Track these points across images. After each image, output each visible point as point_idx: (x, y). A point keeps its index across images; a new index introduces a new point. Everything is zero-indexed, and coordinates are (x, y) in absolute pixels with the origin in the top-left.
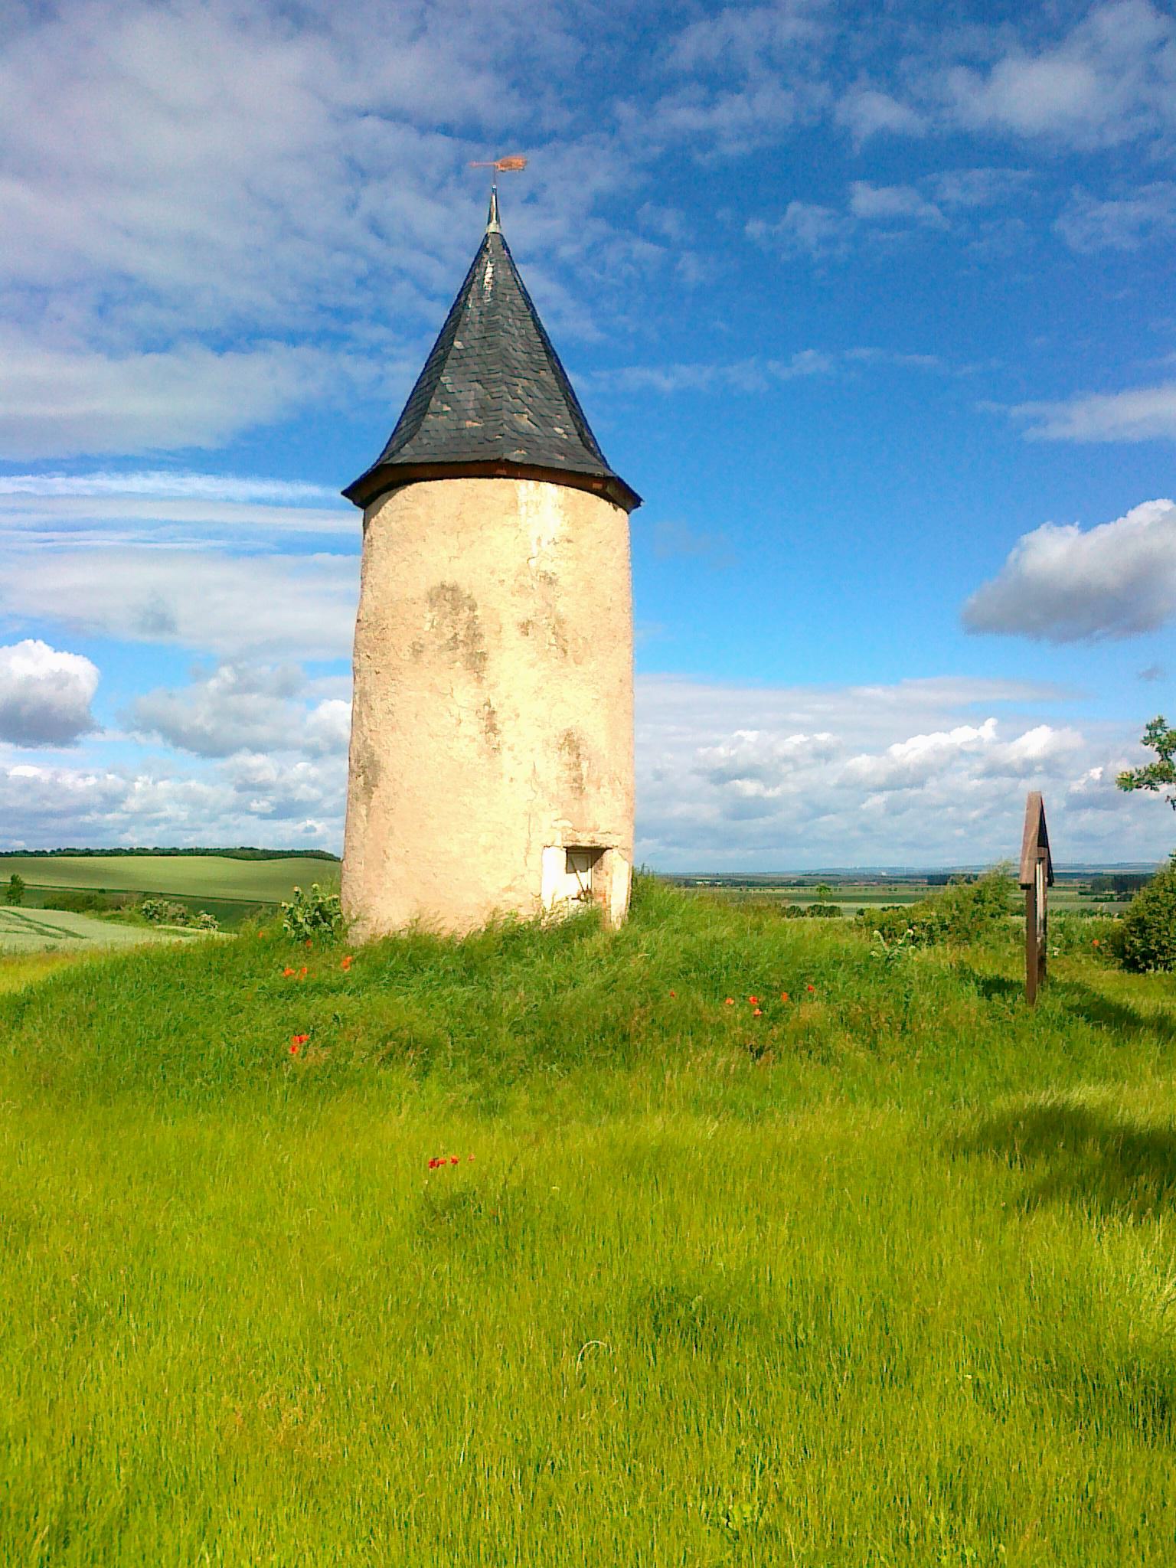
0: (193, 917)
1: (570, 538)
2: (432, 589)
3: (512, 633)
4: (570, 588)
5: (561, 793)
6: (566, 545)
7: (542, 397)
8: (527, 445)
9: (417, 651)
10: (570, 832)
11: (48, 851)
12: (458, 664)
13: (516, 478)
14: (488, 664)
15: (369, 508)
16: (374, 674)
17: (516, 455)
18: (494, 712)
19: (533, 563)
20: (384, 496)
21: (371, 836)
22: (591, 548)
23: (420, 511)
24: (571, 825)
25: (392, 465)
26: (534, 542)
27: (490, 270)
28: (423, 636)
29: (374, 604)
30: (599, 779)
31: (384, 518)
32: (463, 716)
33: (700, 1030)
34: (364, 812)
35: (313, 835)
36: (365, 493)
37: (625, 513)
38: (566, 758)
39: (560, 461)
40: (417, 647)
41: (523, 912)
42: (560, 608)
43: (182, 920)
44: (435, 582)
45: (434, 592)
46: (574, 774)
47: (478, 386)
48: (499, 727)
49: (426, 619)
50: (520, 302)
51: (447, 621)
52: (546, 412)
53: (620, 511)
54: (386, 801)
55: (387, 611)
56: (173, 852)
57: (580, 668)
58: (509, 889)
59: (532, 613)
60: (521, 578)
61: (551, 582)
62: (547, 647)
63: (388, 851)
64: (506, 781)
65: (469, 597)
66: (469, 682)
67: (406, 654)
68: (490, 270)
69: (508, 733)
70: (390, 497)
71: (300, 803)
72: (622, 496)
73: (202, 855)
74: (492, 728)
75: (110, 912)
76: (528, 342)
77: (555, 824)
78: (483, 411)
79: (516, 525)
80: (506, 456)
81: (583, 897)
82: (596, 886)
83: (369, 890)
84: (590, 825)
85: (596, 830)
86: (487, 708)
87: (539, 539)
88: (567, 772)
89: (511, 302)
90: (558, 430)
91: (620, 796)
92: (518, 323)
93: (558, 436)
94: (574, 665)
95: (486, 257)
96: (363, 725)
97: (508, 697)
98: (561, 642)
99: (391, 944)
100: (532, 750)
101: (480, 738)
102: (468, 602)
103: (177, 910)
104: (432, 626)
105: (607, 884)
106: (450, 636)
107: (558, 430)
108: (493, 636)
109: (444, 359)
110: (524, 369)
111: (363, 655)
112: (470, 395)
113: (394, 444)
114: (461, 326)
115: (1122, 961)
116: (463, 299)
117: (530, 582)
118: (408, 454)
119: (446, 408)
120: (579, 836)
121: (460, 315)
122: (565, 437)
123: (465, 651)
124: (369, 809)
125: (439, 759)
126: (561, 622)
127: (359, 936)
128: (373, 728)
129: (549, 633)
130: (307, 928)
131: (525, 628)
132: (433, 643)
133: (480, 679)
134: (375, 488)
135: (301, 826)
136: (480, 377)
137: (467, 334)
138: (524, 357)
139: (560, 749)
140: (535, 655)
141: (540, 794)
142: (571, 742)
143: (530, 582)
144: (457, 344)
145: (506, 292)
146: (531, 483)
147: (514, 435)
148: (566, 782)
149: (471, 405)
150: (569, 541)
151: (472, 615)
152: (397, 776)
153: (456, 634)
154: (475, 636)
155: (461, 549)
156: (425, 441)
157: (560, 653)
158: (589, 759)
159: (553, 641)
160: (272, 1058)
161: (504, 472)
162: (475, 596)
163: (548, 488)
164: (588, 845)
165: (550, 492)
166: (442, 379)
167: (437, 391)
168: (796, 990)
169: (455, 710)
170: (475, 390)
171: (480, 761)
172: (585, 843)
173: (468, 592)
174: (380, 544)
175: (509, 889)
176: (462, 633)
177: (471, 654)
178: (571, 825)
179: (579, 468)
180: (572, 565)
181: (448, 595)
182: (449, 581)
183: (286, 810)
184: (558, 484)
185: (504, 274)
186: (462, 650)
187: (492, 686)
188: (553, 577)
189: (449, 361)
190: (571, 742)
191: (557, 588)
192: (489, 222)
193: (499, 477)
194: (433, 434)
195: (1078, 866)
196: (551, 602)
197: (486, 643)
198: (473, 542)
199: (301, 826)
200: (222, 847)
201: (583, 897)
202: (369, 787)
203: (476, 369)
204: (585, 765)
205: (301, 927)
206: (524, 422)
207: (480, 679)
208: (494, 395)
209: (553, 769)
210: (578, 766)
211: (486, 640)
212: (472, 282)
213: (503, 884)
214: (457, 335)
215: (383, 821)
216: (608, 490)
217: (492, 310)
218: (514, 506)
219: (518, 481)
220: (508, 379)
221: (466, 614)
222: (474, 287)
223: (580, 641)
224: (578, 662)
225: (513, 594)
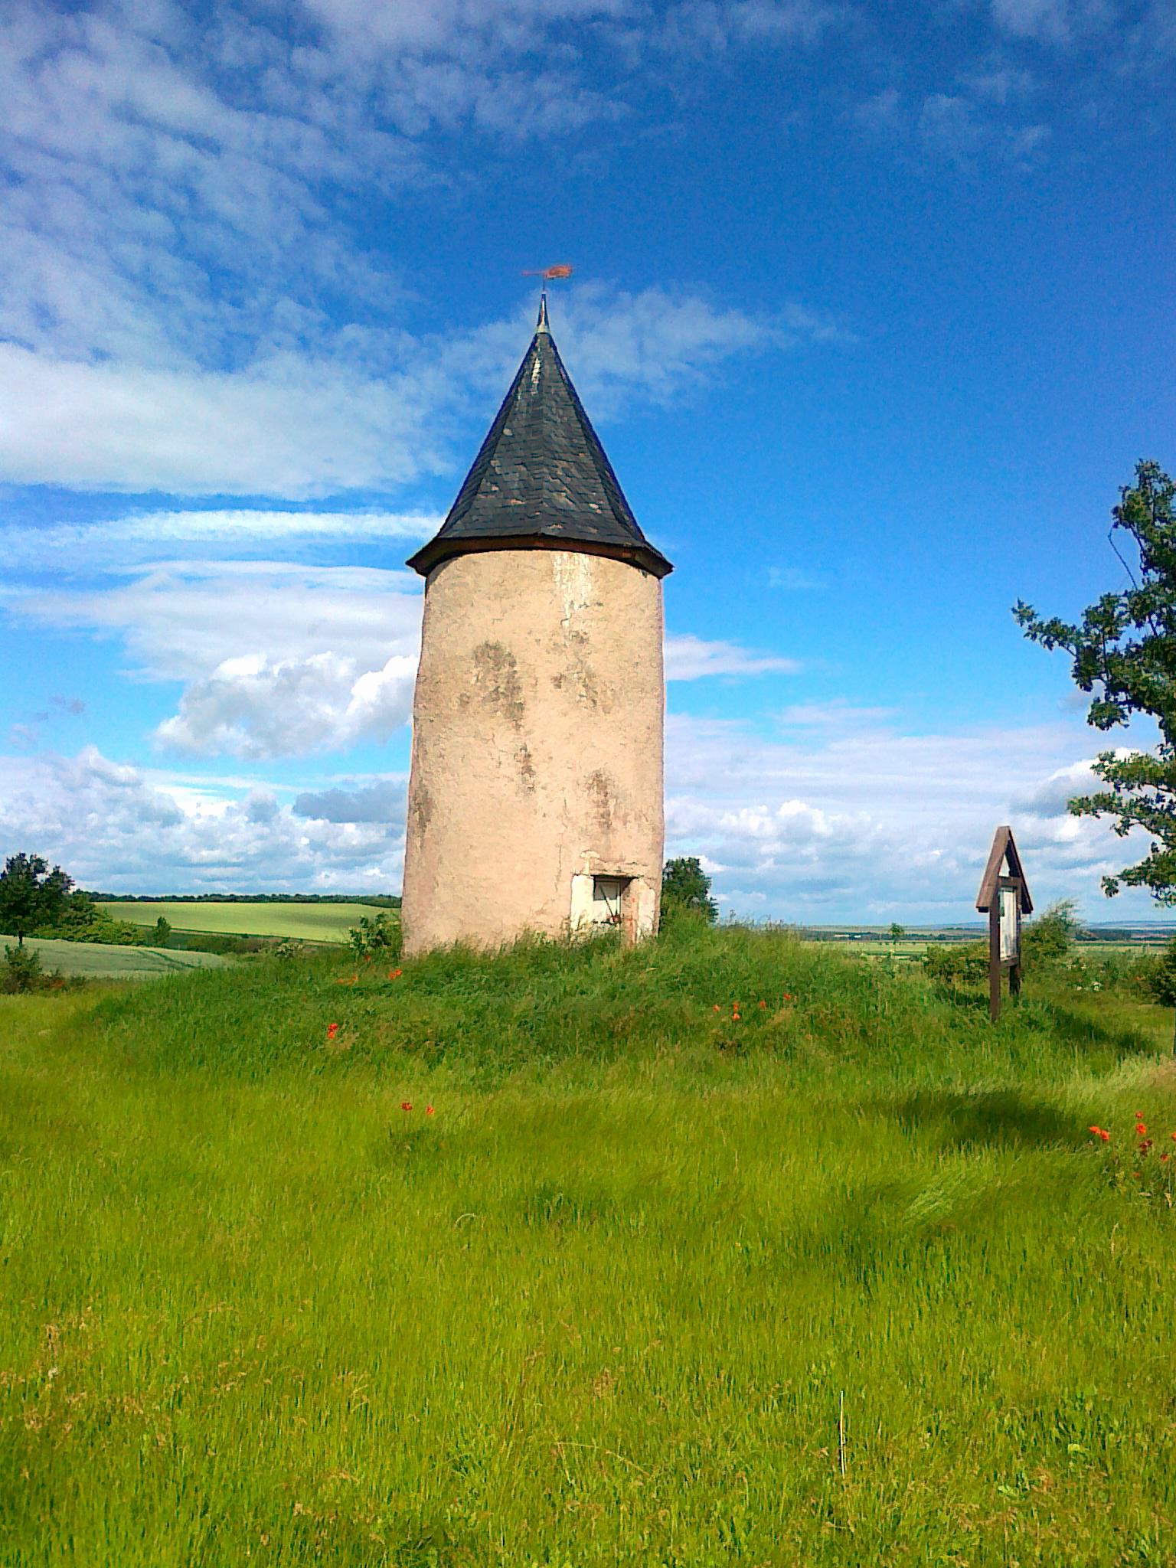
1: (601, 601)
3: (547, 686)
5: (590, 828)
6: (597, 607)
7: (579, 476)
8: (563, 520)
9: (464, 702)
10: (597, 862)
11: (196, 896)
12: (499, 713)
14: (526, 713)
15: (432, 575)
17: (552, 530)
18: (529, 756)
19: (566, 624)
22: (620, 610)
23: (469, 579)
26: (567, 606)
27: (537, 366)
30: (626, 815)
32: (503, 759)
33: (680, 1030)
34: (418, 844)
36: (426, 563)
37: (655, 578)
38: (595, 797)
39: (593, 534)
40: (465, 699)
41: (551, 932)
42: (591, 663)
44: (481, 642)
46: (602, 810)
47: (523, 469)
48: (534, 768)
49: (472, 674)
50: (563, 393)
51: (490, 676)
52: (583, 490)
53: (650, 577)
56: (314, 899)
57: (609, 718)
58: (542, 912)
61: (582, 641)
62: (578, 698)
63: (438, 878)
64: (540, 816)
65: (510, 654)
66: (508, 729)
67: (455, 705)
68: (537, 366)
69: (542, 777)
70: (444, 567)
72: (654, 564)
73: (343, 902)
74: (528, 770)
75: (247, 955)
76: (569, 429)
77: (583, 855)
79: (551, 591)
80: (543, 530)
81: (611, 921)
82: (626, 912)
83: (422, 912)
84: (616, 856)
85: (622, 860)
87: (572, 603)
88: (596, 809)
89: (556, 393)
90: (592, 505)
91: (646, 831)
92: (561, 412)
95: (535, 354)
96: (419, 768)
98: (592, 693)
99: (436, 955)
100: (563, 789)
101: (518, 778)
104: (478, 680)
106: (491, 689)
107: (592, 505)
110: (564, 452)
111: (420, 706)
112: (515, 477)
113: (451, 521)
114: (510, 416)
115: (1159, 996)
116: (514, 391)
117: (563, 641)
118: (459, 530)
119: (495, 488)
120: (606, 866)
122: (599, 511)
123: (505, 702)
124: (423, 840)
126: (591, 676)
127: (411, 947)
129: (580, 686)
131: (558, 681)
132: (478, 695)
133: (518, 727)
137: (515, 423)
138: (564, 442)
139: (589, 788)
141: (570, 827)
142: (599, 783)
143: (563, 641)
144: (507, 432)
145: (551, 384)
146: (566, 554)
147: (553, 512)
148: (595, 818)
149: (516, 485)
150: (600, 604)
155: (504, 612)
156: (474, 518)
158: (616, 798)
160: (310, 1042)
162: (515, 651)
163: (583, 559)
164: (615, 874)
165: (583, 561)
166: (492, 462)
168: (769, 998)
170: (520, 472)
171: (517, 799)
172: (611, 871)
173: (508, 650)
175: (542, 912)
176: (503, 686)
177: (510, 705)
178: (598, 856)
179: (608, 540)
181: (492, 653)
182: (492, 642)
184: (591, 554)
186: (502, 701)
187: (528, 733)
188: (585, 637)
190: (599, 783)
193: (537, 548)
194: (481, 511)
196: (581, 658)
197: (524, 694)
200: (361, 895)
201: (611, 921)
202: (423, 822)
203: (521, 453)
204: (612, 802)
206: (562, 499)
207: (518, 727)
209: (583, 805)
210: (605, 804)
211: (523, 693)
212: (522, 377)
213: (537, 907)
215: (434, 851)
216: (637, 558)
217: (538, 401)
218: (550, 573)
220: (548, 461)
221: (506, 670)
222: (523, 381)
223: (609, 693)
224: (607, 711)
225: (548, 652)
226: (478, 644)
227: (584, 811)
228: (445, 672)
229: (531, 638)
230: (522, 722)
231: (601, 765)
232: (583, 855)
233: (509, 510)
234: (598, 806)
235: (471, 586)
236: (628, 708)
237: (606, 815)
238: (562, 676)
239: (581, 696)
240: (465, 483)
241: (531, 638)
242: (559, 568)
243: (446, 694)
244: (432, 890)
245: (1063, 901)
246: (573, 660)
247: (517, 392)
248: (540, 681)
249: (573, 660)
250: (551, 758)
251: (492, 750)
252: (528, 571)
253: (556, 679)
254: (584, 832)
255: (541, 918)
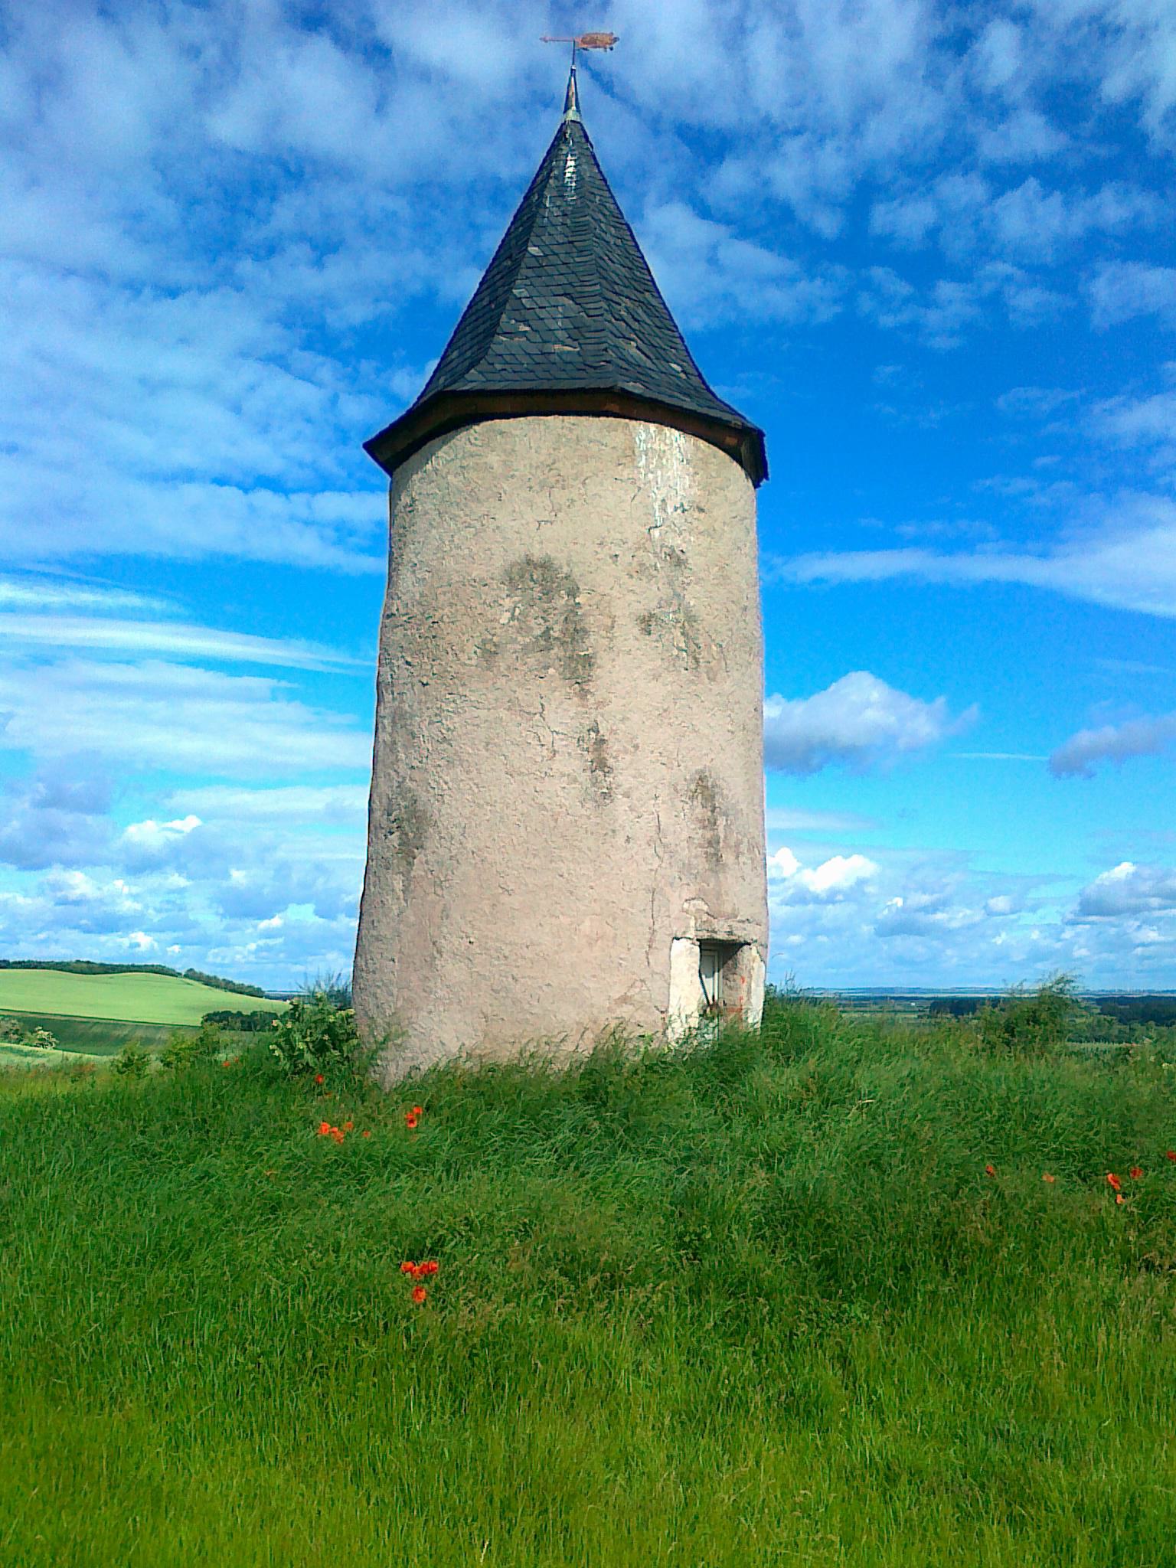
0: (29, 1034)
1: (702, 505)
2: (512, 566)
3: (628, 632)
4: (702, 575)
6: (696, 514)
9: (490, 653)
12: (551, 671)
13: (631, 418)
14: (597, 672)
16: (418, 687)
18: (603, 741)
19: (656, 533)
20: (436, 441)
21: (412, 919)
23: (493, 459)
24: (705, 908)
25: (454, 392)
27: (571, 163)
28: (498, 631)
29: (417, 590)
30: (738, 845)
31: (436, 471)
34: (398, 885)
35: (137, 949)
42: (693, 598)
43: (16, 1036)
44: (517, 554)
45: (515, 570)
46: (709, 834)
48: (611, 762)
51: (535, 611)
54: (436, 868)
55: (441, 598)
58: (624, 1000)
59: (655, 603)
60: (641, 553)
62: (675, 652)
64: (620, 840)
67: (471, 656)
69: (624, 778)
70: (444, 443)
71: (121, 918)
73: (35, 968)
74: (601, 765)
78: (576, 332)
82: (731, 998)
86: (593, 735)
93: (674, 374)
94: (707, 681)
95: (565, 149)
97: (622, 720)
99: (443, 1076)
101: (584, 777)
102: (568, 584)
103: (10, 1026)
104: (513, 618)
105: (744, 995)
106: (537, 632)
108: (603, 633)
109: (513, 271)
112: (559, 313)
118: (474, 380)
121: (534, 216)
122: (683, 376)
123: (561, 654)
125: (522, 807)
126: (691, 619)
127: (393, 1070)
128: (416, 763)
129: (677, 633)
130: (308, 1057)
131: (647, 623)
132: (514, 641)
133: (583, 694)
134: (420, 433)
135: (126, 942)
136: (570, 290)
140: (659, 662)
142: (704, 789)
143: (653, 560)
144: (533, 250)
145: (596, 191)
146: (653, 427)
150: (701, 510)
151: (572, 602)
152: (456, 832)
153: (548, 629)
154: (576, 632)
157: (691, 664)
159: (683, 645)
161: (616, 408)
165: (675, 443)
167: (508, 307)
169: (547, 739)
171: (583, 812)
172: (721, 936)
173: (565, 569)
174: (428, 506)
176: (557, 628)
180: (705, 541)
182: (537, 554)
183: (110, 924)
185: (588, 171)
187: (600, 704)
188: (683, 557)
189: (524, 272)
190: (704, 789)
191: (687, 572)
192: (567, 108)
193: (607, 414)
195: (914, 990)
196: (679, 590)
197: (594, 642)
198: (573, 501)
199: (126, 942)
202: (408, 850)
204: (721, 822)
205: (301, 1055)
206: (632, 349)
207: (583, 694)
208: (592, 313)
211: (592, 639)
212: (548, 177)
214: (533, 239)
219: (634, 422)
221: (563, 602)
226: (512, 558)
227: (685, 835)
228: (451, 605)
229: (604, 553)
230: (591, 687)
231: (706, 762)
232: (686, 905)
233: (553, 358)
234: (704, 827)
235: (498, 469)
236: (736, 675)
237: (713, 842)
238: (651, 616)
239: (680, 649)
240: (455, 333)
241: (604, 553)
242: (643, 446)
243: (454, 639)
244: (430, 962)
245: (1059, 975)
246: (666, 592)
247: (541, 196)
248: (619, 621)
249: (666, 592)
250: (636, 747)
251: (541, 731)
252: (594, 448)
253: (643, 620)
254: (687, 867)
255: (625, 1011)
